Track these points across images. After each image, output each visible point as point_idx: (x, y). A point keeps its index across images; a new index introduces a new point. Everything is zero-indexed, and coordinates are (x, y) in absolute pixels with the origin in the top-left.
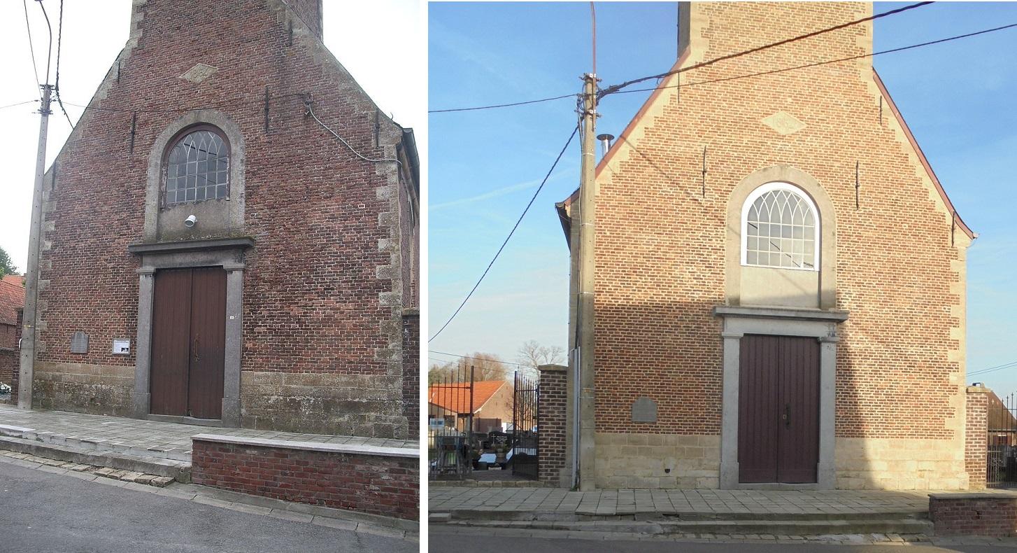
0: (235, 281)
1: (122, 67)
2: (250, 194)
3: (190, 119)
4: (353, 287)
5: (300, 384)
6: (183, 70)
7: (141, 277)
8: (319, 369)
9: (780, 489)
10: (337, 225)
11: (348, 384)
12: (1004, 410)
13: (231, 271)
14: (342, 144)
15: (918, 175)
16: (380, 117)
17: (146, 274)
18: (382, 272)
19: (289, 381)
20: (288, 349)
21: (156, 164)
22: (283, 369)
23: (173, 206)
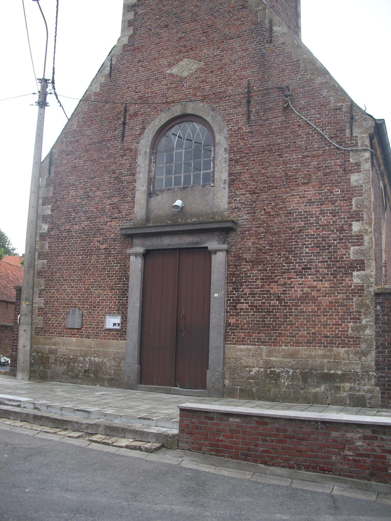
0: (219, 261)
2: (233, 180)
3: (177, 110)
6: (170, 65)
7: (132, 258)
8: (298, 343)
13: (215, 252)
16: (354, 109)
17: (136, 255)
18: (356, 253)
19: (270, 354)
20: (268, 325)
21: (146, 153)
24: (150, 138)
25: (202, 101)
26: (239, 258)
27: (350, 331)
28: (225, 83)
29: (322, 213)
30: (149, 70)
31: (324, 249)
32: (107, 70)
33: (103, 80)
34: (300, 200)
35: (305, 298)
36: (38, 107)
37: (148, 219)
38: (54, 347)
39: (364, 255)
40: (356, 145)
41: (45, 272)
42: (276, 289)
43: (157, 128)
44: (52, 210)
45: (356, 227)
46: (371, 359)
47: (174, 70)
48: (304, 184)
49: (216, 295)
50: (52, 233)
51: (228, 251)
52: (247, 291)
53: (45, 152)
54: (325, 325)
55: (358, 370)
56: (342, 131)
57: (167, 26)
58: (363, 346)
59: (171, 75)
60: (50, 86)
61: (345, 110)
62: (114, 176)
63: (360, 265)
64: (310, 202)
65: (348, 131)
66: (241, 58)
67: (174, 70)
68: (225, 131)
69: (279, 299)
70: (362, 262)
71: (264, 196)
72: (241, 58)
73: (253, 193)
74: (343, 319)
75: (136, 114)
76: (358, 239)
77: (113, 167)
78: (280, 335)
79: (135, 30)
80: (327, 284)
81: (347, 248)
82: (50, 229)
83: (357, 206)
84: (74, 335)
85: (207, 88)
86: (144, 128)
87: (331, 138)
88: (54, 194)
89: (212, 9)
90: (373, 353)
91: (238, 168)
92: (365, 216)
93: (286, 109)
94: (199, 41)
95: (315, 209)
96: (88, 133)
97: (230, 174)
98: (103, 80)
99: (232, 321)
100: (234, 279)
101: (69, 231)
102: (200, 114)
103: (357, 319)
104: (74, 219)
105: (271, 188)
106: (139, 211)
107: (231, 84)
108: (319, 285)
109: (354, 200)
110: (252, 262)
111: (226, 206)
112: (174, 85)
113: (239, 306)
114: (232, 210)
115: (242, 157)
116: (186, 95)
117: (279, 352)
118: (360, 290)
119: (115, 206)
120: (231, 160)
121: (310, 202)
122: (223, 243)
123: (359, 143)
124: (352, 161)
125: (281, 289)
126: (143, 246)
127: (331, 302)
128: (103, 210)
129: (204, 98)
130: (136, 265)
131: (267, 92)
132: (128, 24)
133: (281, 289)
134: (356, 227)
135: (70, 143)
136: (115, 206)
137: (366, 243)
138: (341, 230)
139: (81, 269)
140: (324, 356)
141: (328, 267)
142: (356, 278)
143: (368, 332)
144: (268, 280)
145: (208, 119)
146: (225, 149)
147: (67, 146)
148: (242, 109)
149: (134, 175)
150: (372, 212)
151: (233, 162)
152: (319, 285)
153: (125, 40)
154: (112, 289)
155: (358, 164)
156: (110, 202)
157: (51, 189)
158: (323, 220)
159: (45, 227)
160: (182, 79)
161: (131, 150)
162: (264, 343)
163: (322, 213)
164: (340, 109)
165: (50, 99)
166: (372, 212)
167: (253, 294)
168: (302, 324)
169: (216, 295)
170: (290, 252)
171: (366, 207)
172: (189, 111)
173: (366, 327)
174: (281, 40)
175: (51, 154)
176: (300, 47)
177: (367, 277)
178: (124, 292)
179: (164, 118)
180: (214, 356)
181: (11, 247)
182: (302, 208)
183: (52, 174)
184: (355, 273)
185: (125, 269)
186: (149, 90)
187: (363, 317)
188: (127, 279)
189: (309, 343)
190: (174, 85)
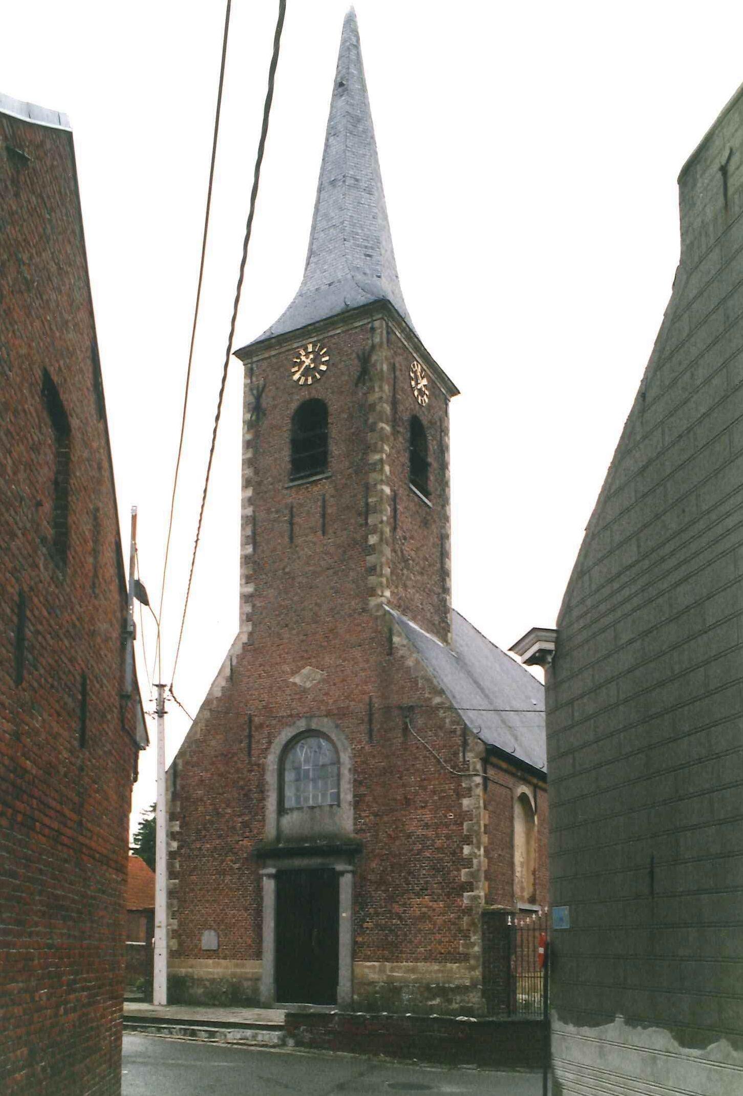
0: (346, 883)
2: (357, 803)
3: (302, 725)
6: (293, 673)
8: (417, 960)
17: (269, 876)
18: (466, 874)
24: (278, 752)
25: (326, 716)
26: (363, 878)
27: (461, 949)
28: (347, 697)
29: (438, 836)
30: (272, 676)
31: (438, 871)
32: (227, 672)
33: (223, 683)
34: (416, 823)
35: (423, 917)
36: (289, 466)
37: (278, 838)
38: (190, 970)
39: (473, 878)
40: (468, 770)
41: (177, 892)
42: (397, 908)
44: (181, 827)
45: (467, 850)
46: (477, 973)
47: (297, 679)
48: (422, 807)
49: (344, 915)
50: (183, 851)
51: (352, 872)
52: (371, 911)
53: (169, 762)
54: (440, 942)
56: (456, 754)
57: (287, 626)
58: (472, 962)
59: (295, 684)
60: (167, 693)
61: (459, 733)
62: (243, 792)
63: (470, 886)
64: (427, 826)
65: (461, 755)
66: (363, 670)
67: (297, 679)
68: (350, 750)
69: (400, 918)
70: (471, 883)
71: (386, 819)
72: (363, 670)
73: (376, 815)
74: (455, 936)
75: (261, 726)
76: (468, 863)
77: (241, 783)
78: (401, 952)
79: (254, 625)
80: (441, 904)
81: (459, 870)
82: (180, 848)
83: (468, 831)
85: (331, 701)
86: (270, 743)
87: (445, 761)
88: (182, 809)
89: (332, 610)
90: (480, 969)
91: (362, 790)
92: (475, 841)
93: (405, 730)
94: (321, 646)
95: (430, 833)
96: (213, 743)
97: (355, 796)
98: (223, 683)
99: (360, 939)
100: (360, 900)
101: (200, 849)
102: (325, 730)
103: (467, 937)
104: (205, 836)
105: (392, 810)
106: (270, 831)
107: (354, 700)
108: (435, 905)
109: (465, 824)
110: (376, 882)
111: (352, 828)
112: (298, 696)
113: (365, 925)
114: (357, 831)
115: (366, 778)
116: (311, 708)
117: (400, 968)
118: (468, 911)
119: (245, 825)
120: (355, 780)
121: (427, 826)
122: (350, 864)
123: (471, 768)
124: (464, 785)
125: (402, 909)
126: (274, 866)
127: (445, 921)
128: (234, 828)
129: (328, 714)
130: (269, 886)
131: (387, 709)
132: (247, 618)
133: (402, 909)
134: (467, 850)
135: (195, 752)
136: (245, 825)
137: (475, 866)
138: (454, 853)
139: (215, 889)
140: (439, 970)
141: (442, 888)
142: (466, 899)
143: (476, 949)
144: (391, 899)
145: (333, 737)
146: (350, 770)
147: (191, 757)
148: (364, 727)
150: (405, 619)
151: (357, 783)
152: (435, 905)
153: (245, 638)
154: (246, 909)
155: (470, 789)
156: (240, 820)
157: (178, 803)
158: (438, 843)
159: (175, 845)
160: (305, 691)
161: (258, 765)
162: (387, 960)
163: (438, 836)
164: (454, 731)
165: (169, 706)
166: (405, 619)
167: (357, 685)
168: (420, 942)
169: (344, 915)
170: (410, 873)
171: (476, 831)
172: (314, 727)
173: (474, 944)
174: (401, 652)
175: (175, 764)
177: (476, 898)
178: (259, 913)
179: (286, 734)
180: (344, 973)
182: (420, 832)
183: (178, 787)
184: (465, 894)
185: (259, 889)
186: (273, 700)
187: (471, 935)
188: (262, 898)
189: (425, 960)
190: (298, 696)
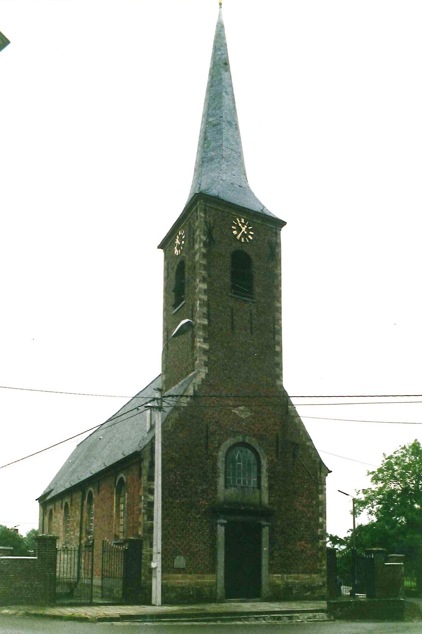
0: (266, 531)
1: (196, 389)
2: (270, 488)
3: (240, 438)
4: (310, 538)
5: (291, 579)
6: (234, 407)
7: (218, 525)
8: (298, 573)
9: (202, 123)
10: (305, 509)
11: (309, 578)
12: (298, 468)
13: (264, 526)
14: (308, 472)
15: (153, 565)
16: (323, 467)
17: (222, 524)
18: (321, 531)
19: (287, 578)
20: (283, 566)
21: (223, 461)
22: (285, 573)
23: (231, 486)
35: (302, 551)
43: (228, 446)
49: (265, 549)
55: (321, 584)
58: (323, 573)
84: (180, 573)
130: (221, 530)
149: (215, 473)
151: (270, 478)
176: (282, 386)
181: (334, 536)
184: (320, 541)
